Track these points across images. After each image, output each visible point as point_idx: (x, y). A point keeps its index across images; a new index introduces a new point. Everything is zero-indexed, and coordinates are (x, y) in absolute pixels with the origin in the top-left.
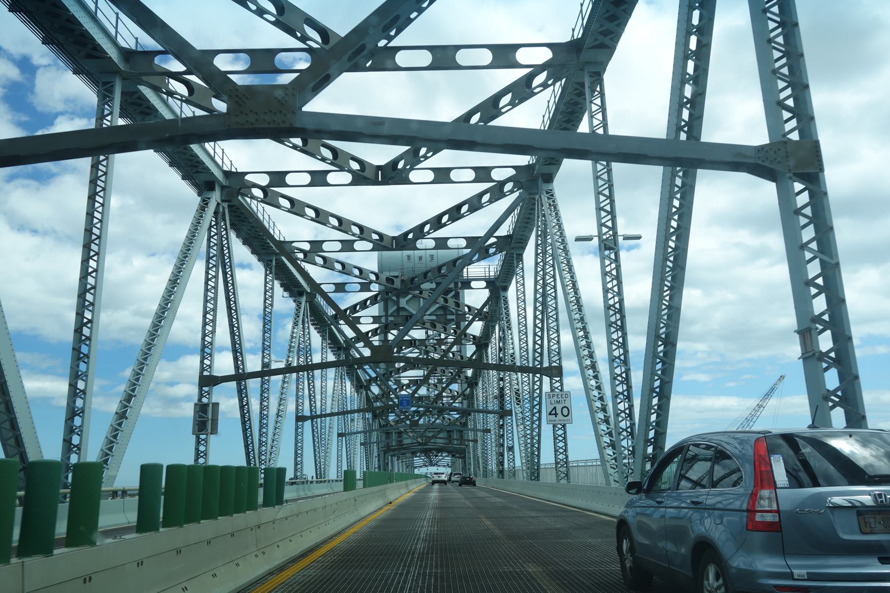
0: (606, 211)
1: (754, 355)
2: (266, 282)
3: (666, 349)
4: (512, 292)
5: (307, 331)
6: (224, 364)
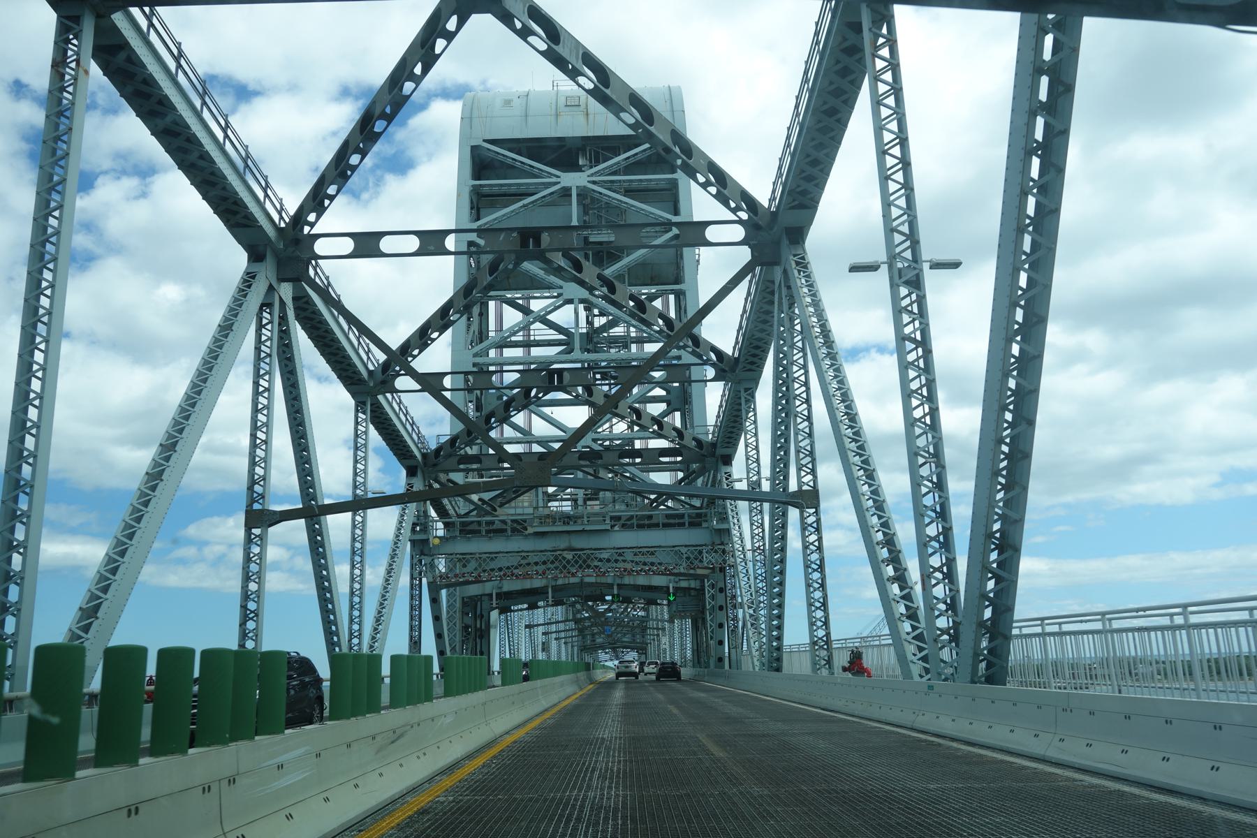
1: (1069, 498)
2: (357, 423)
3: (1003, 557)
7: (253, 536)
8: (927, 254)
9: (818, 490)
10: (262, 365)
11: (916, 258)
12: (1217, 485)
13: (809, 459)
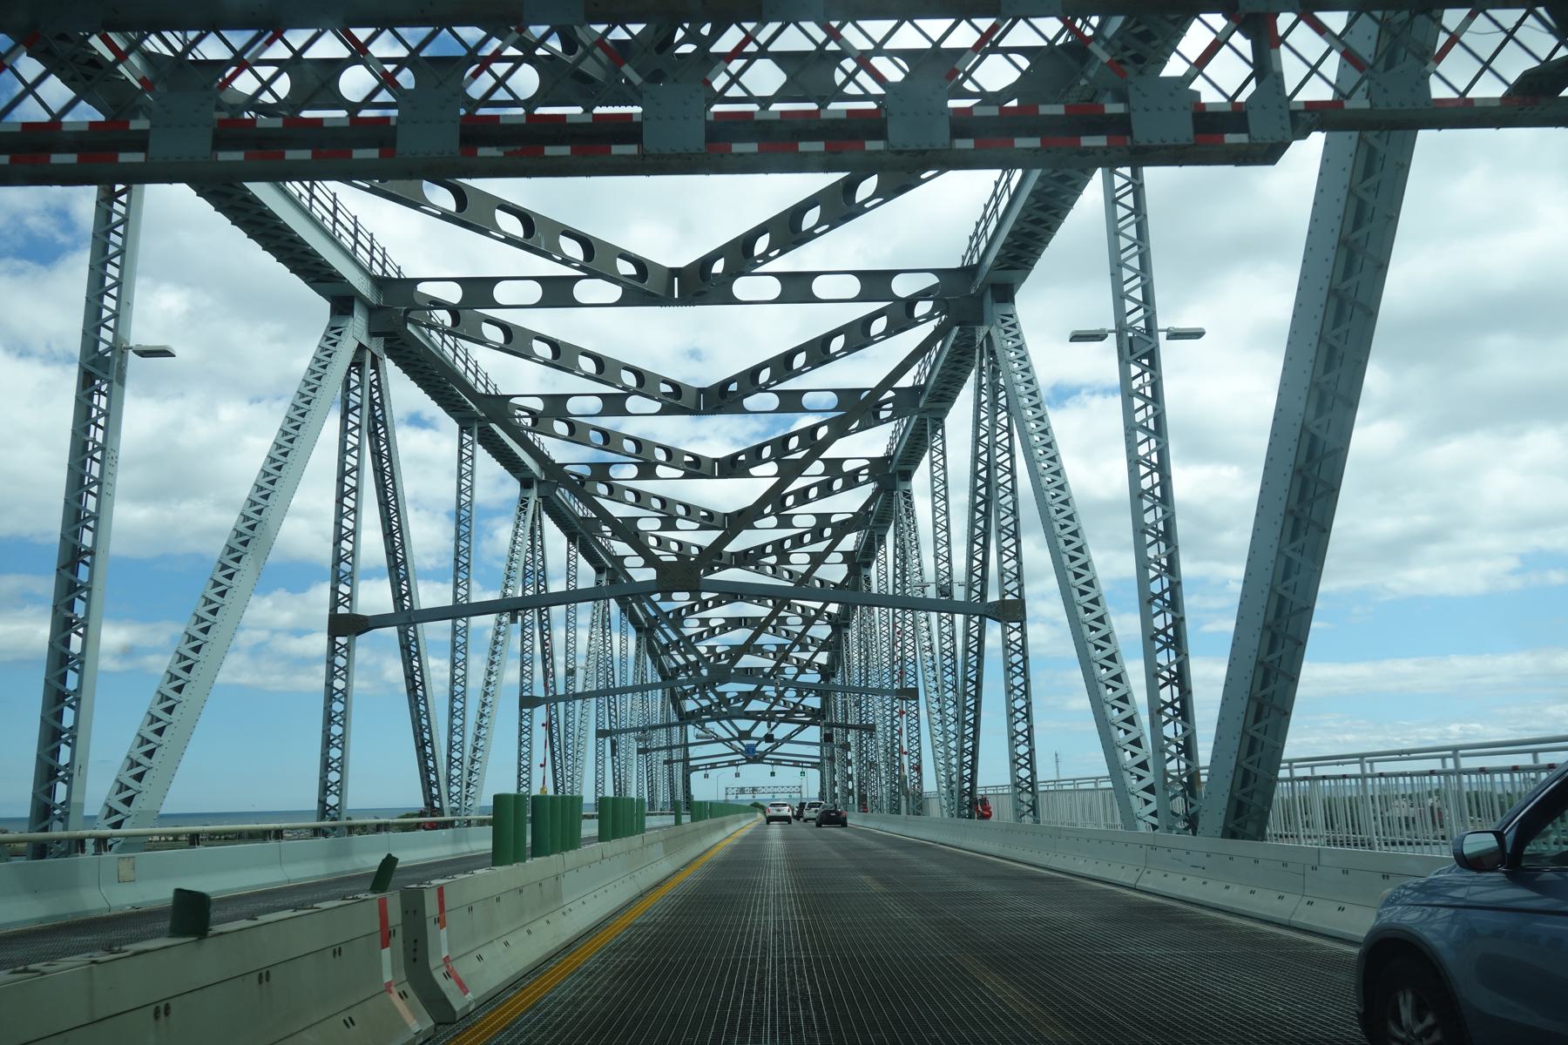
0: (971, 681)
2: (461, 446)
4: (921, 479)
5: (539, 543)
6: (375, 597)
7: (337, 646)
8: (1163, 323)
9: (1024, 601)
10: (350, 437)
11: (1150, 329)
12: (1513, 572)
13: (1011, 519)
